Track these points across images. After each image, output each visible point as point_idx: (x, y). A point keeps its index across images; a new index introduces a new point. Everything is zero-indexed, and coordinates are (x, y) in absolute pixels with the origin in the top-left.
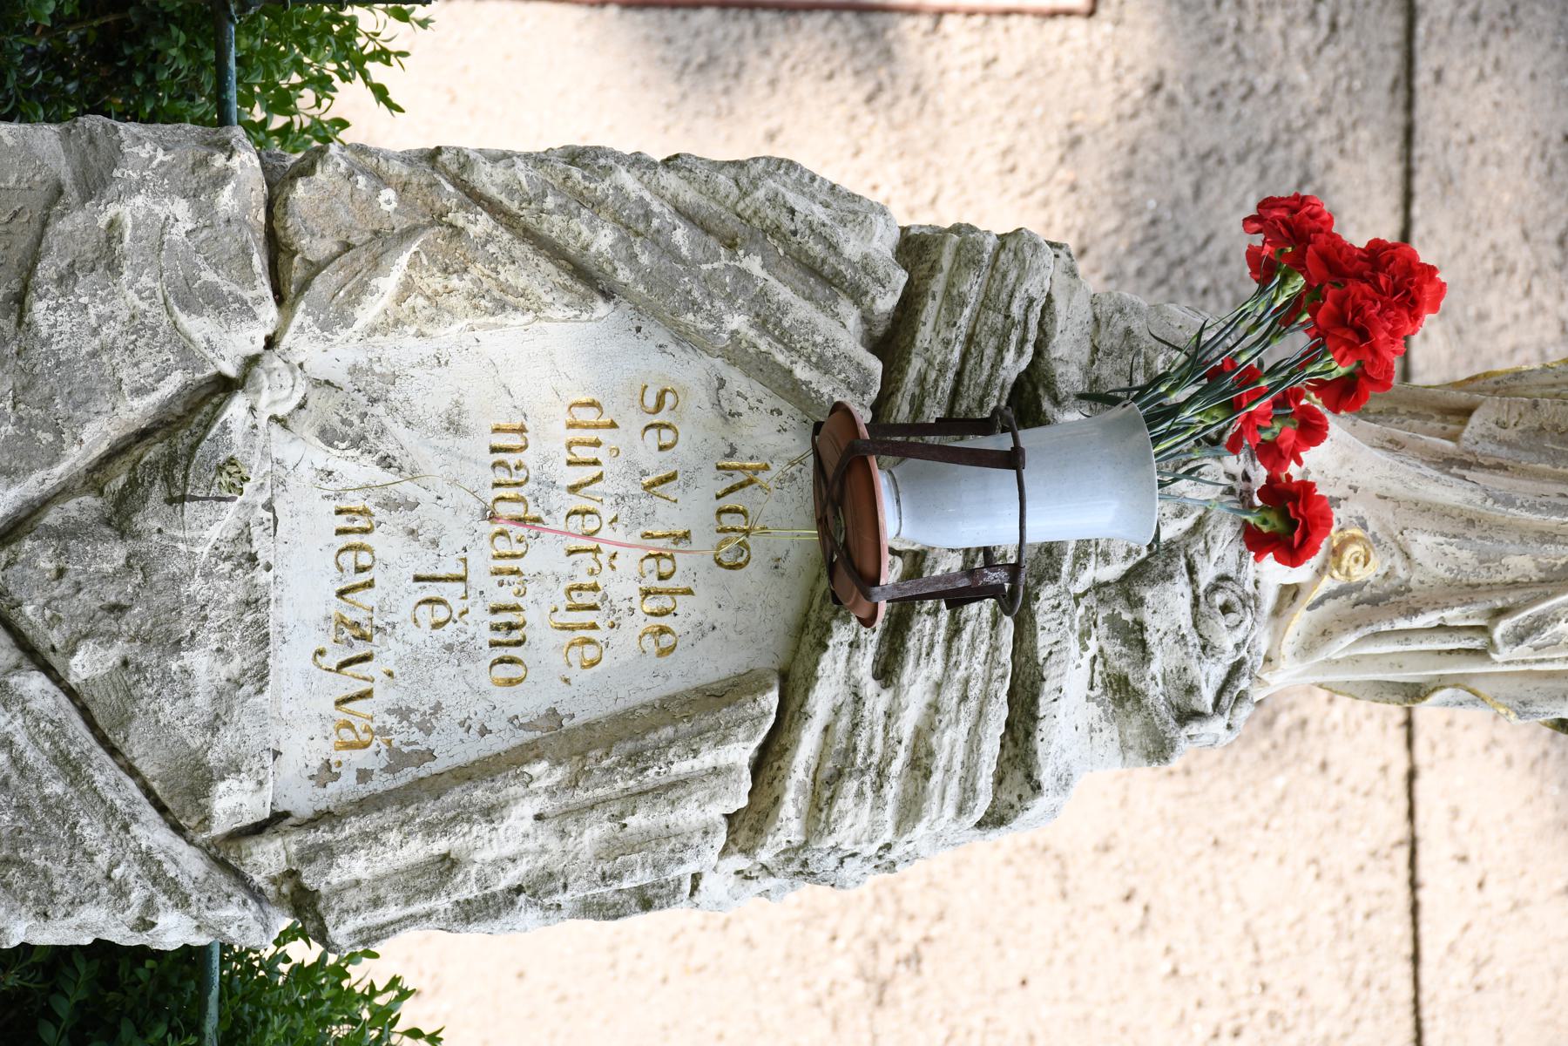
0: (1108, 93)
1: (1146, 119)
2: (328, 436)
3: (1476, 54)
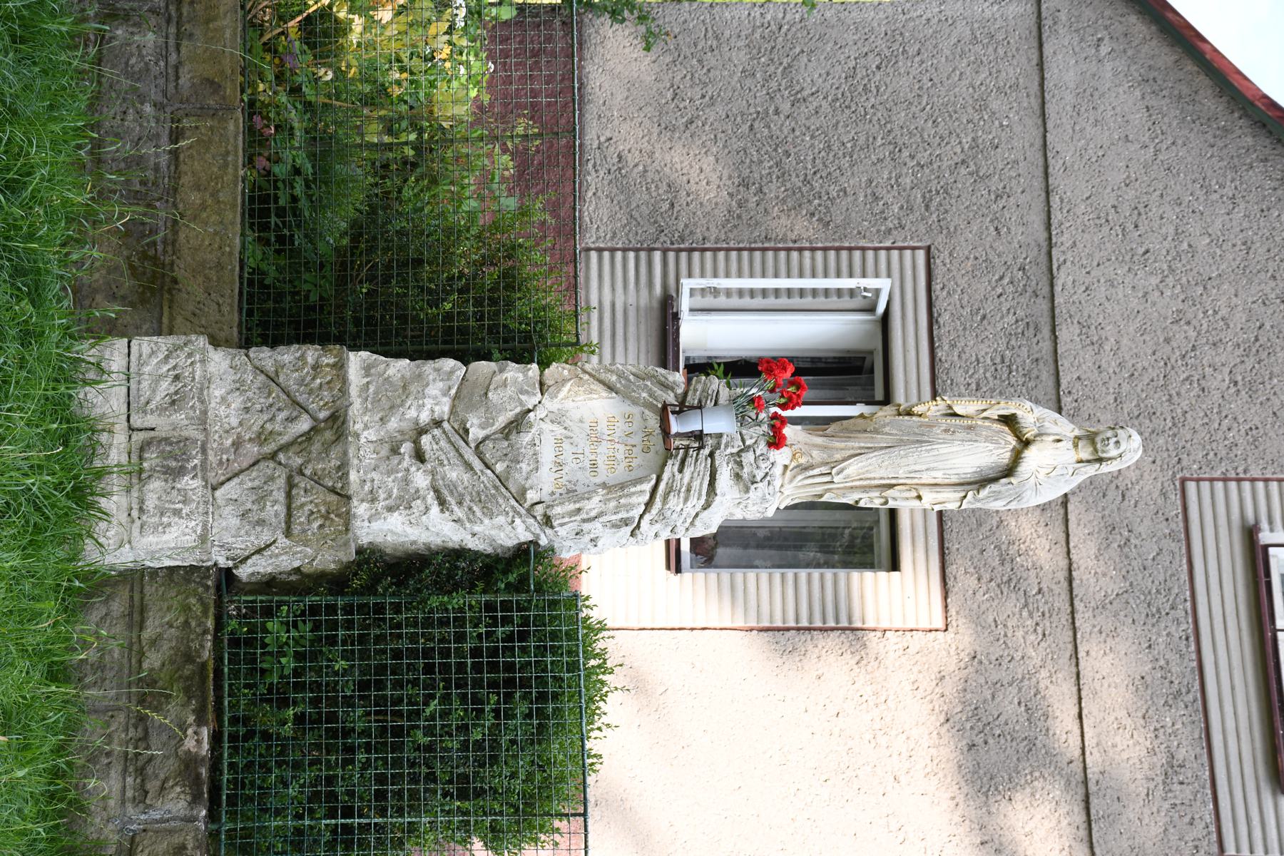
0: (954, 659)
1: (970, 669)
2: (552, 422)
3: (1102, 645)
